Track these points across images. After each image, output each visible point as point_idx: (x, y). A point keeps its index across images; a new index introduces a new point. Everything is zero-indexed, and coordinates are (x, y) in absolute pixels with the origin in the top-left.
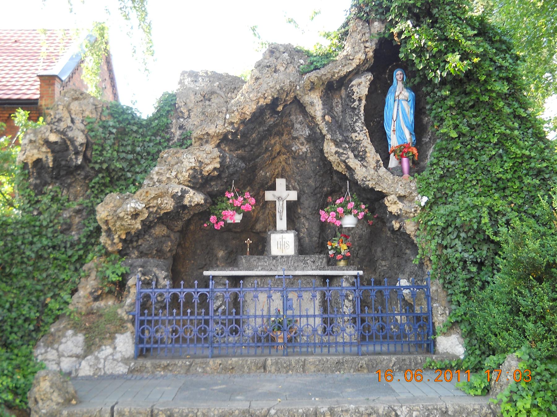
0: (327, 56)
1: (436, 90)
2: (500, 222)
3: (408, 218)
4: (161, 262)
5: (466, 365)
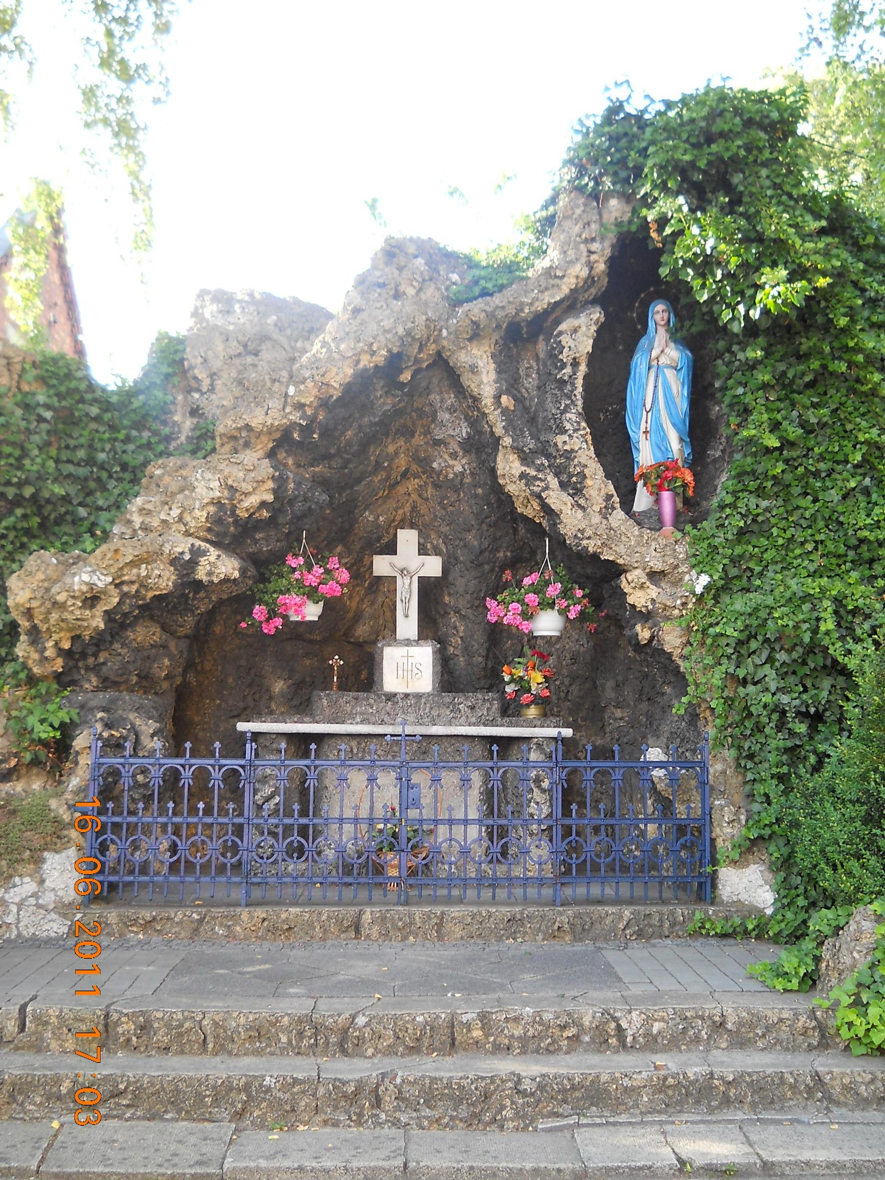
0: (510, 268)
1: (735, 348)
2: (859, 632)
3: (668, 618)
4: (148, 701)
5: (776, 929)
